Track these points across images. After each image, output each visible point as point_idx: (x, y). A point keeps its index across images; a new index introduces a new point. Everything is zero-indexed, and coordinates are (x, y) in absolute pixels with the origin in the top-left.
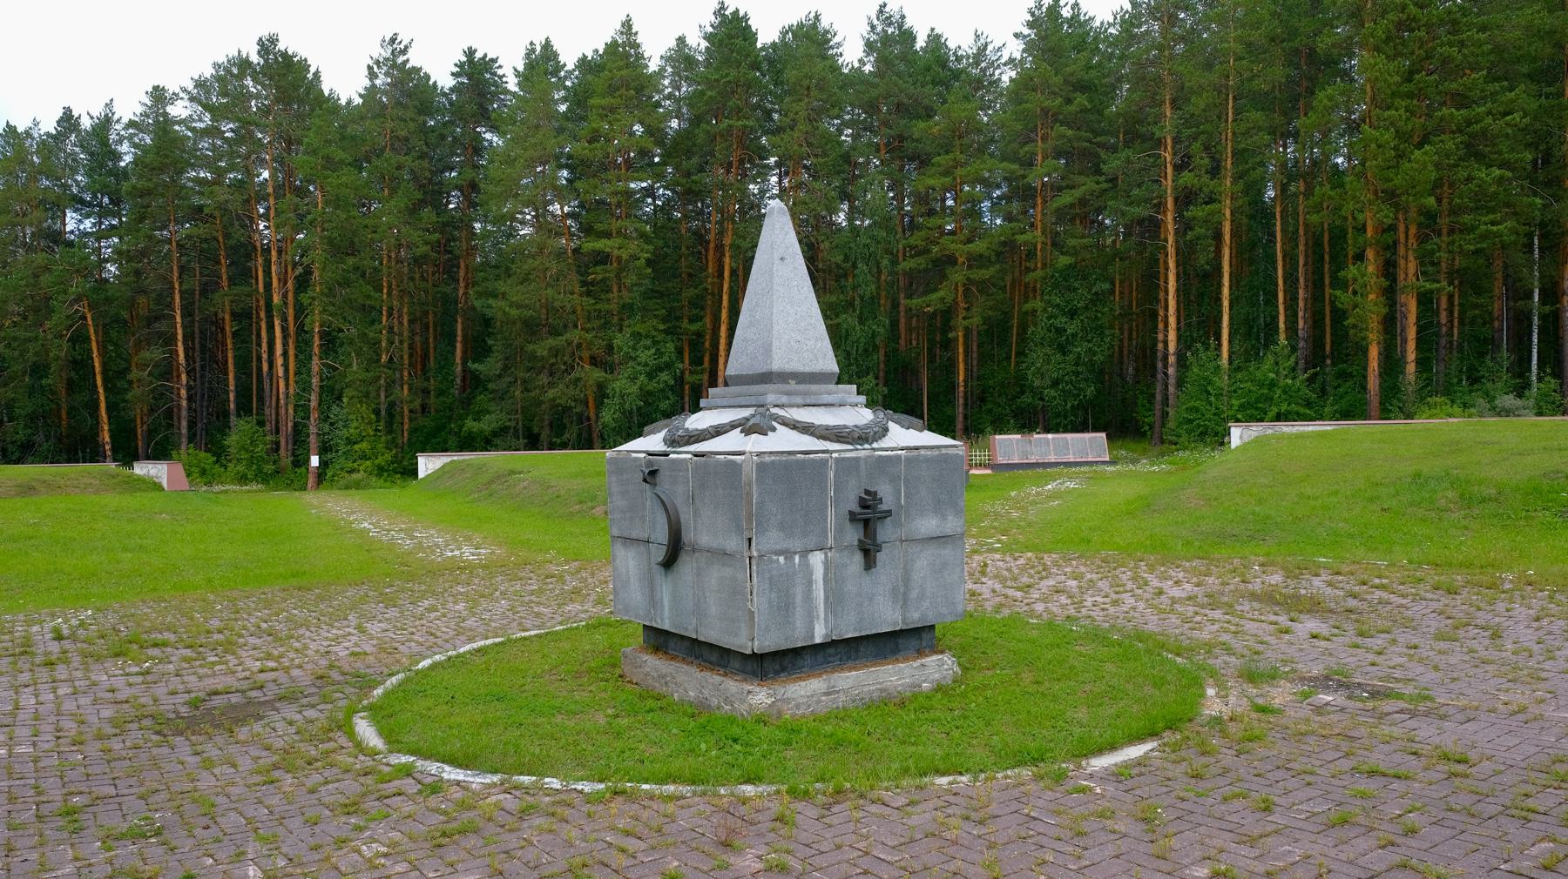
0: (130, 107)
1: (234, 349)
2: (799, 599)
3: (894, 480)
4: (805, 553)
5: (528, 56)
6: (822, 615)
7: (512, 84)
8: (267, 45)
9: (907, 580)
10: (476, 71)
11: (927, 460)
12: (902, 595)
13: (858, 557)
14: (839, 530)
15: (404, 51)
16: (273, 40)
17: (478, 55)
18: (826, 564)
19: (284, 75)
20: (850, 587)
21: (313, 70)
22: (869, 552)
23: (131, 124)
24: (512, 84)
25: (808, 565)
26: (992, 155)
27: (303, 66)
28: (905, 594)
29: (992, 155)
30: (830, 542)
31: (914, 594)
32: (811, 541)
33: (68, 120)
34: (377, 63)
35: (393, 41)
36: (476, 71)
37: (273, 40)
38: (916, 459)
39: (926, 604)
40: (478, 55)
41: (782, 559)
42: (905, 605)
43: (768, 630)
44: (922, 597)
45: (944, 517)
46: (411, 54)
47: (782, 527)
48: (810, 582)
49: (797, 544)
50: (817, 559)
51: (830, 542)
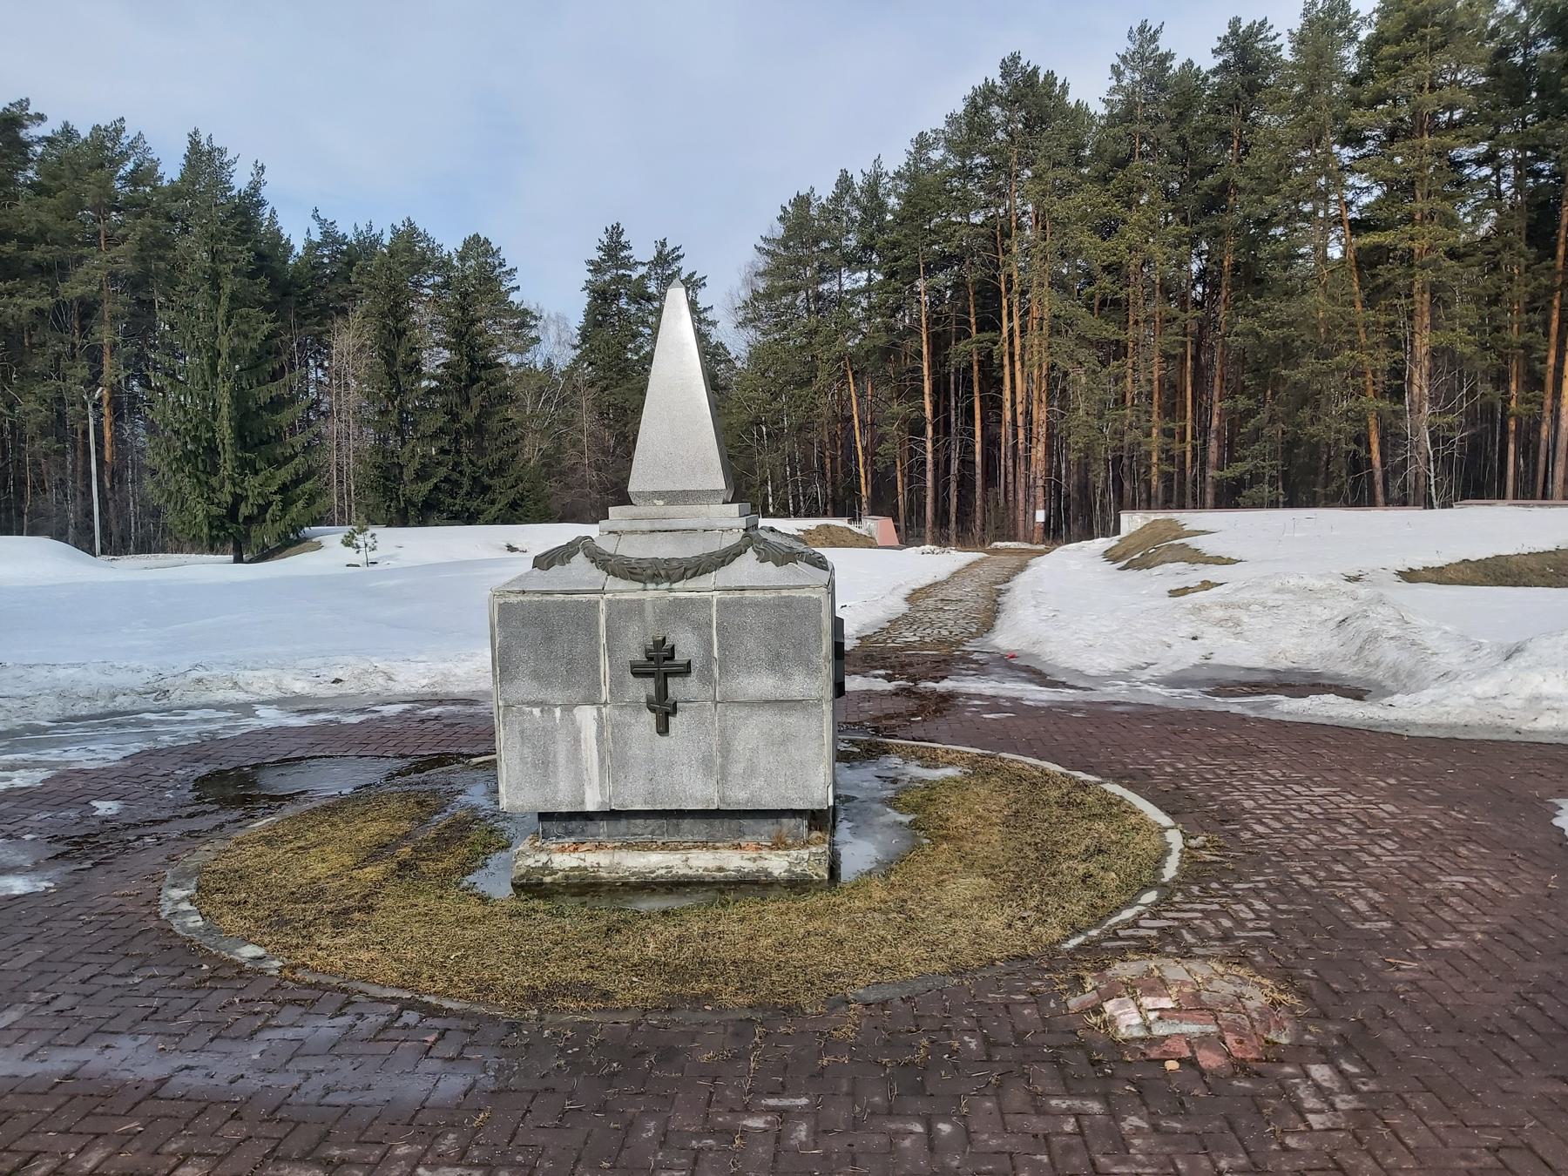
0: (896, 160)
1: (981, 390)
2: (562, 758)
3: (701, 628)
4: (568, 708)
5: (1306, 12)
6: (596, 780)
7: (1287, 55)
8: (1009, 66)
9: (726, 749)
10: (1244, 49)
11: (755, 604)
12: (718, 764)
13: (649, 718)
14: (617, 685)
15: (1153, 38)
16: (1015, 58)
17: (1244, 26)
18: (600, 720)
19: (1029, 96)
20: (637, 751)
21: (1059, 82)
22: (664, 711)
23: (899, 175)
24: (1287, 55)
25: (573, 722)
26: (1422, 38)
27: (1051, 78)
28: (723, 767)
29: (1422, 38)
30: (605, 694)
31: (737, 769)
32: (576, 693)
33: (845, 182)
34: (1124, 59)
35: (1142, 30)
36: (1244, 49)
37: (1015, 58)
38: (739, 603)
39: (759, 783)
40: (1244, 26)
41: (536, 711)
42: (723, 778)
43: (519, 788)
44: (751, 772)
45: (787, 676)
46: (1162, 37)
47: (536, 675)
48: (577, 741)
49: (556, 695)
50: (586, 716)
51: (605, 694)
